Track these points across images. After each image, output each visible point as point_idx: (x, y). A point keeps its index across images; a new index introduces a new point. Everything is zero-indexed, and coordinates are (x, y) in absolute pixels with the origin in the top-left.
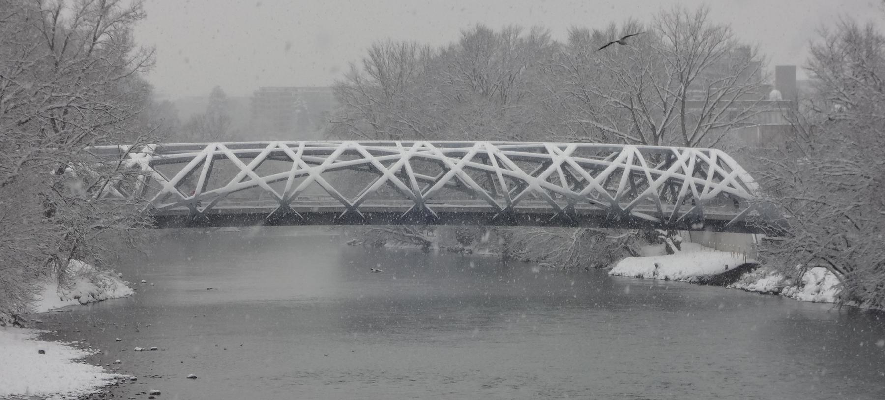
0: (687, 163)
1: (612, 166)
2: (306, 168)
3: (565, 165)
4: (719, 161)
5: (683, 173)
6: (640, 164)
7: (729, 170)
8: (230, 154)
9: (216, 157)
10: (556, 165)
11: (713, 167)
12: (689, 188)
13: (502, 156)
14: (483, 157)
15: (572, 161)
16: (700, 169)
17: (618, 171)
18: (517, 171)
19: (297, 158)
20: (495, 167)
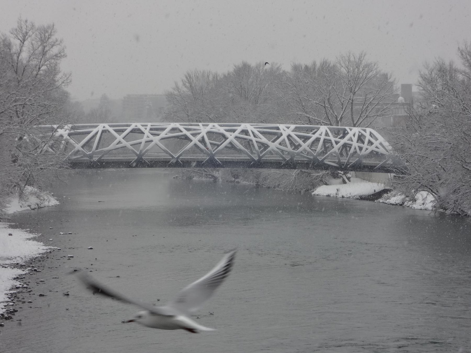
0: (354, 135)
1: (314, 137)
2: (151, 137)
3: (289, 136)
4: (371, 134)
5: (352, 141)
6: (329, 136)
7: (376, 139)
8: (111, 129)
9: (103, 132)
10: (284, 136)
11: (368, 137)
12: (355, 149)
13: (256, 131)
14: (245, 132)
15: (293, 134)
16: (361, 139)
17: (318, 140)
18: (264, 140)
19: (147, 132)
20: (252, 137)
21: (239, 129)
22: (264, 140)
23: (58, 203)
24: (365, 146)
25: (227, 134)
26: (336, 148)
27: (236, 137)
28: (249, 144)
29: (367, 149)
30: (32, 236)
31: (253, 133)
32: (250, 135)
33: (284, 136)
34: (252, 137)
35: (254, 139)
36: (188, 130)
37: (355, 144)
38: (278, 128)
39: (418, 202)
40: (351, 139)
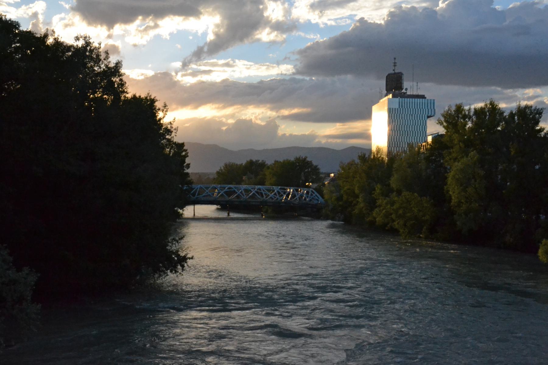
15: (279, 191)
20: (262, 191)
27: (256, 192)
35: (263, 193)
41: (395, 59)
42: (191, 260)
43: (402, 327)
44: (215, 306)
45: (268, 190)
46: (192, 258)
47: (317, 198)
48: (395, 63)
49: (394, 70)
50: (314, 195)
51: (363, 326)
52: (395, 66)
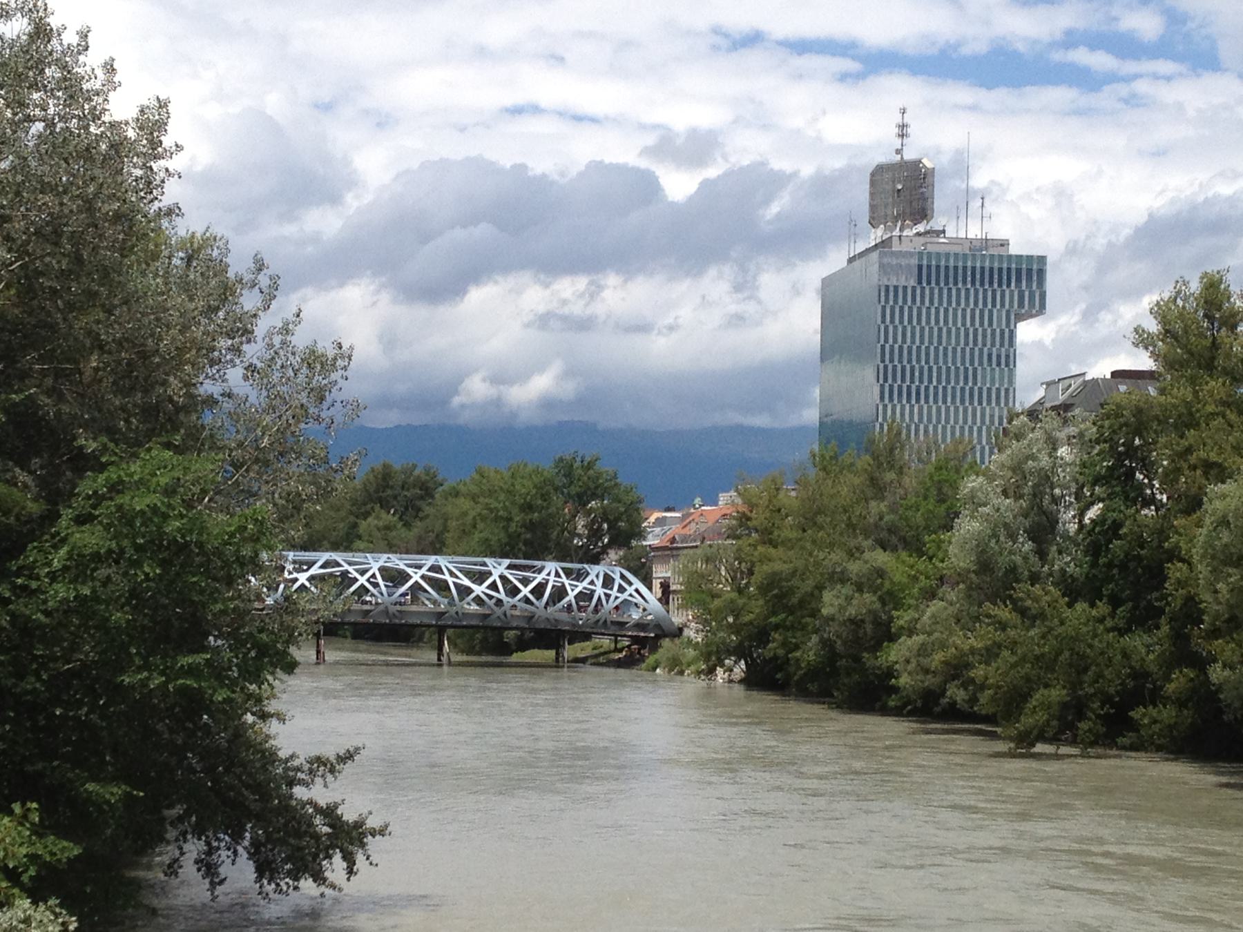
3: (502, 577)
7: (630, 584)
10: (495, 577)
11: (618, 581)
13: (450, 566)
14: (436, 568)
15: (507, 573)
18: (466, 582)
20: (447, 577)
21: (429, 564)
22: (466, 582)
23: (1131, 714)
24: (614, 593)
25: (410, 571)
26: (571, 596)
27: (423, 577)
28: (442, 587)
29: (617, 598)
30: (1224, 780)
31: (449, 570)
32: (443, 573)
33: (495, 577)
34: (346, 567)
35: (450, 580)
36: (350, 564)
37: (599, 591)
38: (485, 564)
39: (192, 862)
40: (592, 583)
41: (903, 112)
42: (378, 837)
43: (15, 685)
44: (1187, 910)
45: (468, 574)
46: (382, 831)
47: (639, 600)
48: (902, 136)
49: (898, 152)
50: (630, 590)
51: (1137, 76)
52: (903, 126)
